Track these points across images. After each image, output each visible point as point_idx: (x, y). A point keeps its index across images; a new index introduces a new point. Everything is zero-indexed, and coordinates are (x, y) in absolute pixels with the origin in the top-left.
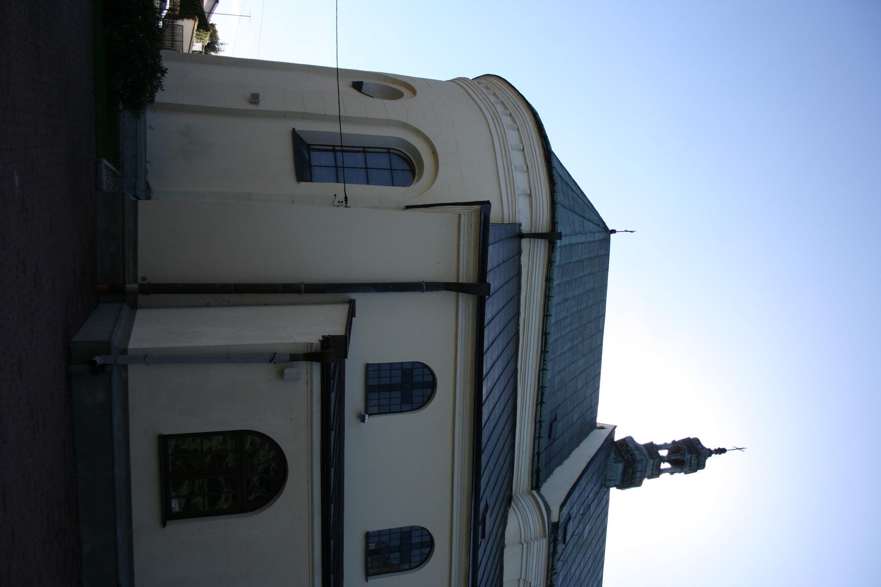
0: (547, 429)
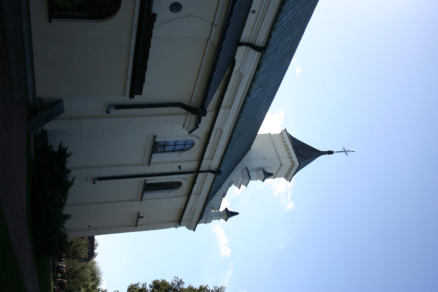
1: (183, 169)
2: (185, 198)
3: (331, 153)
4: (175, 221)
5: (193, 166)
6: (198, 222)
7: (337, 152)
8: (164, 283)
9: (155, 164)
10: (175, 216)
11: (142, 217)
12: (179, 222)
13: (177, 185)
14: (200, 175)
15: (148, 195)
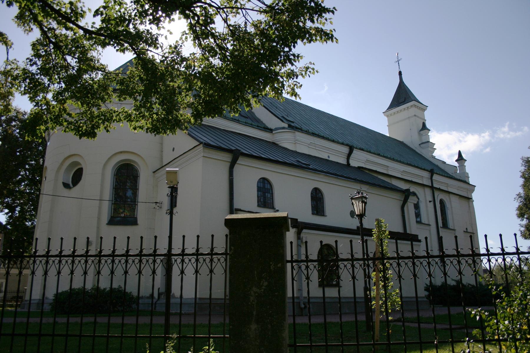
0: (243, 118)
1: (431, 199)
2: (451, 195)
3: (400, 73)
4: (469, 202)
5: (428, 191)
6: (469, 184)
7: (399, 68)
8: (520, 209)
9: (429, 221)
10: (464, 202)
11: (467, 229)
12: (469, 199)
13: (442, 202)
14: (435, 185)
15: (451, 225)
